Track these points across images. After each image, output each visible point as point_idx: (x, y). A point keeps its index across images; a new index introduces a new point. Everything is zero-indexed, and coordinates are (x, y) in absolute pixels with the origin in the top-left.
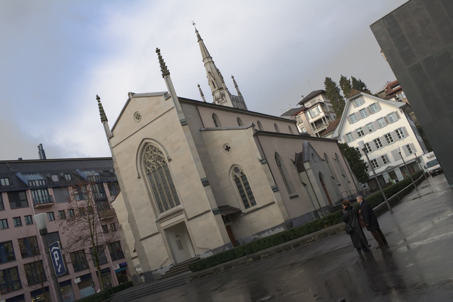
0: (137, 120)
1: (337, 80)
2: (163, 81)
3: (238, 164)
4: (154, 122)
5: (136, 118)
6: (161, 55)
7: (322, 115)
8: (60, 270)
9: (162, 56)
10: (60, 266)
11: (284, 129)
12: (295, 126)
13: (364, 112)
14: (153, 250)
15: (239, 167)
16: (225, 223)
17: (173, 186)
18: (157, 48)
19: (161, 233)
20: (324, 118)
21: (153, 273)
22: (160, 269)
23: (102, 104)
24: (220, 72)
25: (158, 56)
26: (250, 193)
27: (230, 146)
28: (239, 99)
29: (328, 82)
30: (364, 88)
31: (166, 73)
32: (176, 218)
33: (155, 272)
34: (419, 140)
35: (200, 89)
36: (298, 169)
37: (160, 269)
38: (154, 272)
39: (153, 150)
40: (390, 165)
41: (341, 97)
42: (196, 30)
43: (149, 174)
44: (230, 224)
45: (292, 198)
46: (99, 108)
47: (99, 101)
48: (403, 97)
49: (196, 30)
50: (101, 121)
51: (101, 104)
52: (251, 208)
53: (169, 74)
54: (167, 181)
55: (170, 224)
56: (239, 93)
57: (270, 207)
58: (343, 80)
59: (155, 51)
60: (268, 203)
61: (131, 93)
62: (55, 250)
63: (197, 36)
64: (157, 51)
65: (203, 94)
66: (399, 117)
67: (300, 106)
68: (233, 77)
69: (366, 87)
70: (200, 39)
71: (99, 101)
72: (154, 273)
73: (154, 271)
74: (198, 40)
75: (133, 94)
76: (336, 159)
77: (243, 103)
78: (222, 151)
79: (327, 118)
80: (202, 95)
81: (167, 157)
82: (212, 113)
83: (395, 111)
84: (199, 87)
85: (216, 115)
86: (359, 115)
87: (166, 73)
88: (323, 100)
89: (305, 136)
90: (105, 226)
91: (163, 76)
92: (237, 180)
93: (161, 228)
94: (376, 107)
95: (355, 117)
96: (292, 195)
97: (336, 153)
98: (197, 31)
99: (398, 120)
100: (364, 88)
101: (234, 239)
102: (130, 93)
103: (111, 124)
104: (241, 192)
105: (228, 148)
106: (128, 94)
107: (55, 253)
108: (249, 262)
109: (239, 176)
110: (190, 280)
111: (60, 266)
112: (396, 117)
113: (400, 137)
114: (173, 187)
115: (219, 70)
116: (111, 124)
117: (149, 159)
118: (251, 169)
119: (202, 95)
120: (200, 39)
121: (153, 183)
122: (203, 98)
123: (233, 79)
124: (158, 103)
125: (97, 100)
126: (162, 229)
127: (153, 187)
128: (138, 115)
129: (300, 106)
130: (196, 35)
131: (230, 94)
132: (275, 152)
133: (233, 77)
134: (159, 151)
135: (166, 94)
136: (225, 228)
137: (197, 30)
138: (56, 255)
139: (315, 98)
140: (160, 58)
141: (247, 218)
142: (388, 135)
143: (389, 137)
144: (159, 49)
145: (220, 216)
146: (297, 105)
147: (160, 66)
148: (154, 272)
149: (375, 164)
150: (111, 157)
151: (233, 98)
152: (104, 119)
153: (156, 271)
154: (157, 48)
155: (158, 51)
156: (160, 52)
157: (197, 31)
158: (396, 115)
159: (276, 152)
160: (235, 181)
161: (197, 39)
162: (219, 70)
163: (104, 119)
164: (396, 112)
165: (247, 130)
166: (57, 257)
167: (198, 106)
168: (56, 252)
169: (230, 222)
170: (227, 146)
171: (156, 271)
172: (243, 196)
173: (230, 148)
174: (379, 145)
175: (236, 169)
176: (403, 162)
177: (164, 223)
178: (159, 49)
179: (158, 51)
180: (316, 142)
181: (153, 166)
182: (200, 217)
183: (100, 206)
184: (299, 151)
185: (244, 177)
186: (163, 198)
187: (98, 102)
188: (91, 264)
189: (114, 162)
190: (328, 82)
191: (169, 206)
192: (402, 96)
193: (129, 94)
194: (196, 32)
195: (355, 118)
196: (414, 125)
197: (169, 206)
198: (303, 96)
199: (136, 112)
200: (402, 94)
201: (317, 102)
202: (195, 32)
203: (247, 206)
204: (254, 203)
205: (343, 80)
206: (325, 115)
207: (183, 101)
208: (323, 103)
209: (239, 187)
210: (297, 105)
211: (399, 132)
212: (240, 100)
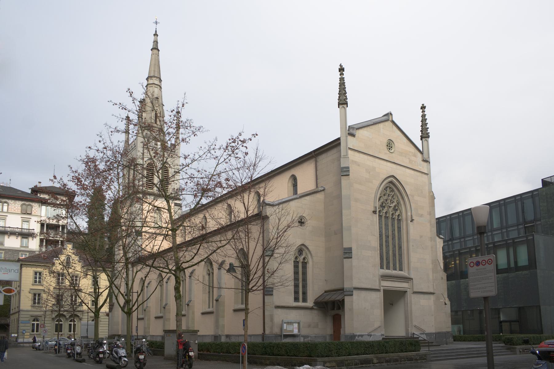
4: (406, 169)
14: (365, 308)
21: (356, 338)
22: (368, 335)
32: (393, 283)
33: (360, 337)
37: (368, 335)
38: (358, 337)
42: (156, 31)
47: (342, 74)
49: (156, 31)
55: (401, 287)
63: (154, 42)
64: (421, 108)
70: (155, 48)
71: (342, 74)
72: (358, 338)
73: (359, 336)
78: (310, 224)
98: (156, 35)
120: (155, 48)
124: (415, 156)
125: (339, 71)
130: (152, 38)
137: (157, 33)
144: (424, 105)
147: (347, 99)
148: (358, 337)
149: (38, 278)
153: (362, 337)
154: (423, 105)
157: (156, 35)
171: (362, 337)
176: (134, 291)
177: (386, 282)
178: (424, 105)
179: (423, 107)
182: (423, 295)
183: (223, 199)
186: (388, 253)
187: (340, 75)
188: (38, 281)
194: (154, 35)
199: (393, 140)
202: (153, 34)
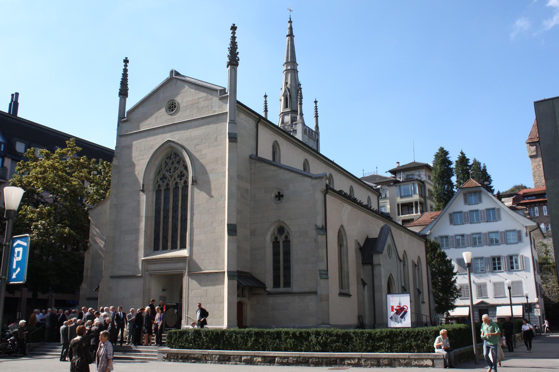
0: (170, 111)
1: (454, 157)
2: (226, 71)
3: (285, 222)
5: (169, 108)
6: (236, 35)
7: (416, 197)
8: (16, 276)
9: (236, 37)
10: (19, 270)
11: (361, 195)
12: (377, 200)
13: (492, 214)
14: (124, 297)
15: (286, 227)
16: (238, 296)
17: (185, 219)
18: (234, 25)
19: (143, 279)
20: (416, 203)
23: (128, 71)
24: (301, 88)
25: (232, 35)
26: (288, 268)
27: (283, 194)
28: (314, 135)
29: (442, 156)
30: (486, 183)
31: (233, 61)
34: (537, 281)
35: (266, 101)
36: (363, 260)
39: (175, 160)
40: (485, 300)
41: (451, 184)
43: (158, 192)
44: (245, 300)
45: (341, 294)
46: (123, 74)
48: (535, 214)
49: (290, 19)
50: (118, 93)
51: (127, 70)
52: (282, 289)
53: (237, 65)
54: (180, 210)
56: (317, 127)
57: (308, 298)
58: (463, 160)
59: (230, 27)
60: (307, 290)
61: (175, 71)
62: (19, 246)
65: (268, 109)
66: (520, 239)
67: (389, 175)
68: (317, 102)
69: (490, 183)
74: (288, 34)
75: (177, 74)
76: (416, 263)
77: (317, 141)
79: (421, 205)
80: (266, 111)
81: (192, 176)
82: (274, 140)
83: (518, 229)
84: (266, 98)
85: (278, 145)
86: (468, 217)
87: (233, 61)
88: (424, 178)
89: (387, 217)
90: (473, 203)
91: (229, 64)
92: (276, 243)
93: (146, 271)
94: (494, 214)
95: (477, 216)
96: (343, 291)
97: (420, 256)
99: (517, 243)
100: (486, 183)
101: (242, 322)
102: (173, 70)
103: (131, 103)
104: (276, 261)
105: (279, 196)
106: (170, 70)
107: (17, 250)
108: (257, 361)
109: (281, 239)
110: (164, 357)
111: (19, 270)
112: (516, 237)
113: (512, 268)
114: (185, 221)
115: (301, 85)
116: (131, 103)
117: (167, 171)
118: (300, 236)
119: (266, 111)
121: (158, 205)
122: (266, 114)
123: (316, 104)
125: (124, 62)
126: (147, 272)
127: (157, 210)
128: (173, 104)
129: (389, 175)
131: (304, 124)
132: (341, 224)
133: (317, 102)
134: (184, 165)
135: (223, 91)
136: (236, 304)
138: (19, 252)
139: (415, 172)
140: (125, 70)
141: (271, 300)
142: (497, 258)
143: (497, 261)
145: (235, 282)
146: (386, 172)
150: (114, 149)
151: (307, 130)
152: (124, 93)
154: (126, 58)
155: (126, 61)
156: (236, 30)
157: (290, 22)
158: (518, 235)
159: (343, 225)
160: (273, 244)
161: (287, 32)
162: (301, 85)
163: (124, 93)
164: (519, 232)
165: (315, 181)
166: (18, 256)
167: (260, 123)
168: (21, 249)
169: (245, 297)
170: (279, 193)
172: (276, 268)
173: (282, 196)
174: (497, 266)
175: (281, 230)
178: (128, 59)
179: (126, 61)
180: (398, 231)
181: (168, 182)
184: (375, 233)
185: (287, 242)
189: (115, 157)
190: (442, 156)
191: (169, 244)
192: (534, 212)
193: (172, 72)
195: (476, 217)
196: (536, 258)
197: (169, 244)
198: (398, 163)
200: (534, 210)
201: (416, 177)
203: (276, 284)
204: (288, 284)
205: (463, 160)
206: (420, 199)
207: (241, 108)
208: (423, 182)
209: (276, 254)
210: (386, 172)
211: (514, 261)
212: (314, 137)
